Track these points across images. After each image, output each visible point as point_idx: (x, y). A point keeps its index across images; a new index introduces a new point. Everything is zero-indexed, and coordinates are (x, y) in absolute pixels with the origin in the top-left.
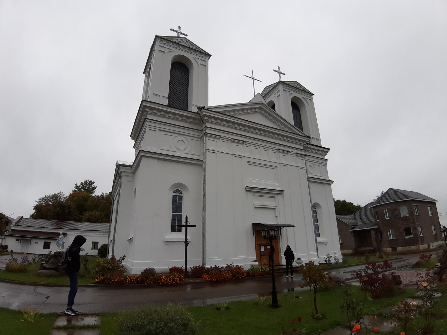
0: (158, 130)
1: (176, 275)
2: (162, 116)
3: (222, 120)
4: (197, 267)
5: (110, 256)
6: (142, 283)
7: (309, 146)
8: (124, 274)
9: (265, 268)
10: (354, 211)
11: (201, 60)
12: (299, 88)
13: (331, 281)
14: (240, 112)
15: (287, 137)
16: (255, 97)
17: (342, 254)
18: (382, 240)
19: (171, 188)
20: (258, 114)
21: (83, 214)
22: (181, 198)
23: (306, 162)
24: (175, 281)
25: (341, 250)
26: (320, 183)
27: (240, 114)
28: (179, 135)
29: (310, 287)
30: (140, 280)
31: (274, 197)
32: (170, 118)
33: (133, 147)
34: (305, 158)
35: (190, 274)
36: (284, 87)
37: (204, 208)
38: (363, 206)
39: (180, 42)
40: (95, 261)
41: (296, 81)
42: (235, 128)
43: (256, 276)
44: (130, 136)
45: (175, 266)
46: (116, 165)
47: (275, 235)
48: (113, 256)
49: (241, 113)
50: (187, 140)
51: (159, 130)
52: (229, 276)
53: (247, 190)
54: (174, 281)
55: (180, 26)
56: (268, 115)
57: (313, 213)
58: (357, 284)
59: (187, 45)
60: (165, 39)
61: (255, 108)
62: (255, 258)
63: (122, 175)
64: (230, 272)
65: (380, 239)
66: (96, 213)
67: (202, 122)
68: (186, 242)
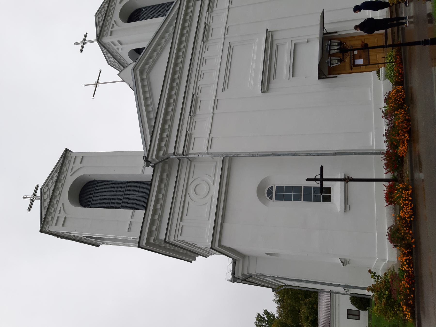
1: (399, 195)
3: (163, 130)
4: (385, 163)
5: (370, 293)
6: (412, 247)
8: (397, 274)
9: (391, 56)
11: (74, 164)
12: (105, 10)
14: (149, 103)
16: (124, 81)
19: (264, 203)
20: (150, 75)
22: (279, 189)
24: (407, 196)
28: (188, 192)
30: (406, 249)
31: (277, 47)
32: (163, 207)
33: (207, 257)
35: (396, 174)
36: (107, 35)
37: (294, 154)
39: (48, 195)
40: (377, 316)
41: (95, 15)
42: (174, 110)
44: (191, 262)
45: (383, 196)
46: (233, 283)
47: (340, 44)
48: (368, 289)
49: (151, 102)
51: (181, 221)
52: (402, 113)
54: (408, 198)
59: (52, 185)
60: (45, 219)
61: (142, 80)
62: (373, 74)
63: (248, 273)
64: (395, 112)
66: (304, 311)
67: (167, 160)
68: (347, 180)
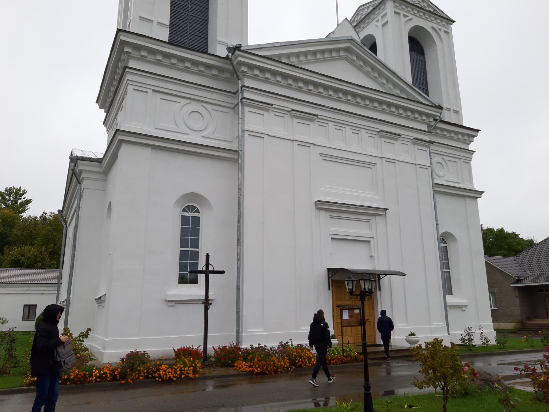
0: (151, 90)
1: (188, 363)
2: (158, 63)
3: (274, 73)
4: (226, 346)
6: (123, 380)
8: (87, 364)
9: (350, 351)
12: (426, 7)
13: (475, 379)
14: (310, 57)
15: (397, 107)
17: (494, 330)
19: (178, 202)
21: (5, 252)
22: (196, 221)
23: (433, 155)
25: (493, 322)
27: (309, 62)
28: (193, 102)
29: (435, 387)
30: (119, 373)
31: (367, 221)
33: (103, 124)
34: (429, 148)
35: (213, 359)
36: (396, 7)
38: (539, 241)
42: (299, 89)
43: (333, 364)
44: (97, 103)
45: (186, 345)
46: (70, 158)
49: (310, 60)
50: (206, 111)
52: (285, 364)
53: (320, 206)
57: (440, 251)
58: (527, 388)
61: (338, 50)
64: (286, 356)
66: (31, 251)
67: (235, 76)
68: (207, 303)
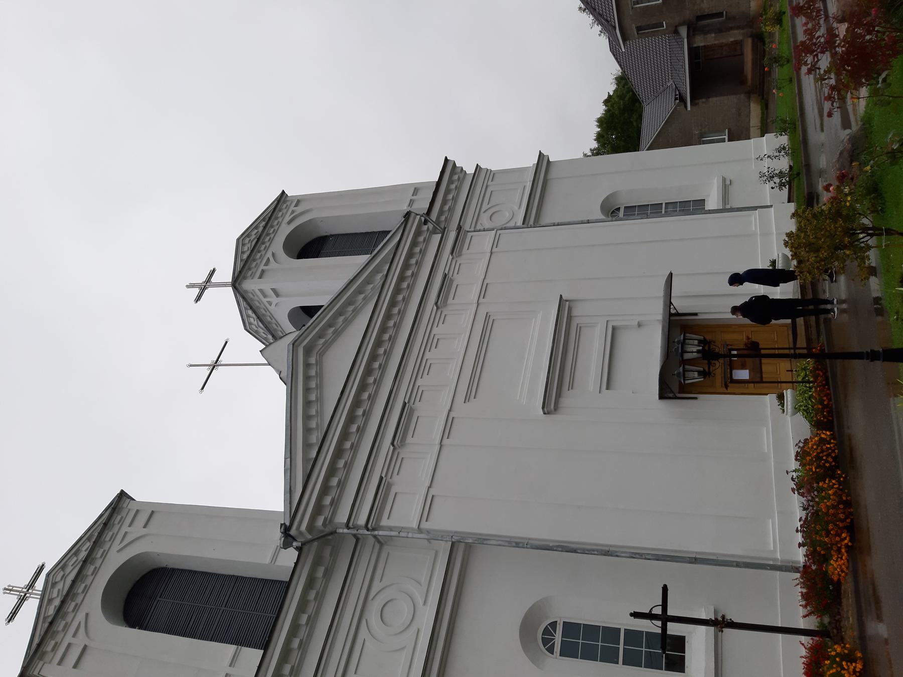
1: (834, 670)
3: (332, 471)
4: (802, 592)
7: (434, 216)
9: (805, 369)
10: (631, 93)
11: (130, 526)
12: (258, 231)
14: (313, 412)
17: (763, 136)
18: (726, 12)
22: (570, 628)
23: (478, 227)
26: (544, 193)
27: (320, 413)
31: (579, 329)
32: (304, 646)
34: (468, 232)
35: (826, 620)
41: (238, 240)
42: (361, 431)
49: (317, 411)
52: (833, 488)
53: (552, 407)
55: (5, 589)
56: (332, 330)
60: (39, 645)
61: (307, 366)
62: (770, 400)
64: (819, 484)
65: (721, 19)
67: (330, 537)
68: (720, 624)
